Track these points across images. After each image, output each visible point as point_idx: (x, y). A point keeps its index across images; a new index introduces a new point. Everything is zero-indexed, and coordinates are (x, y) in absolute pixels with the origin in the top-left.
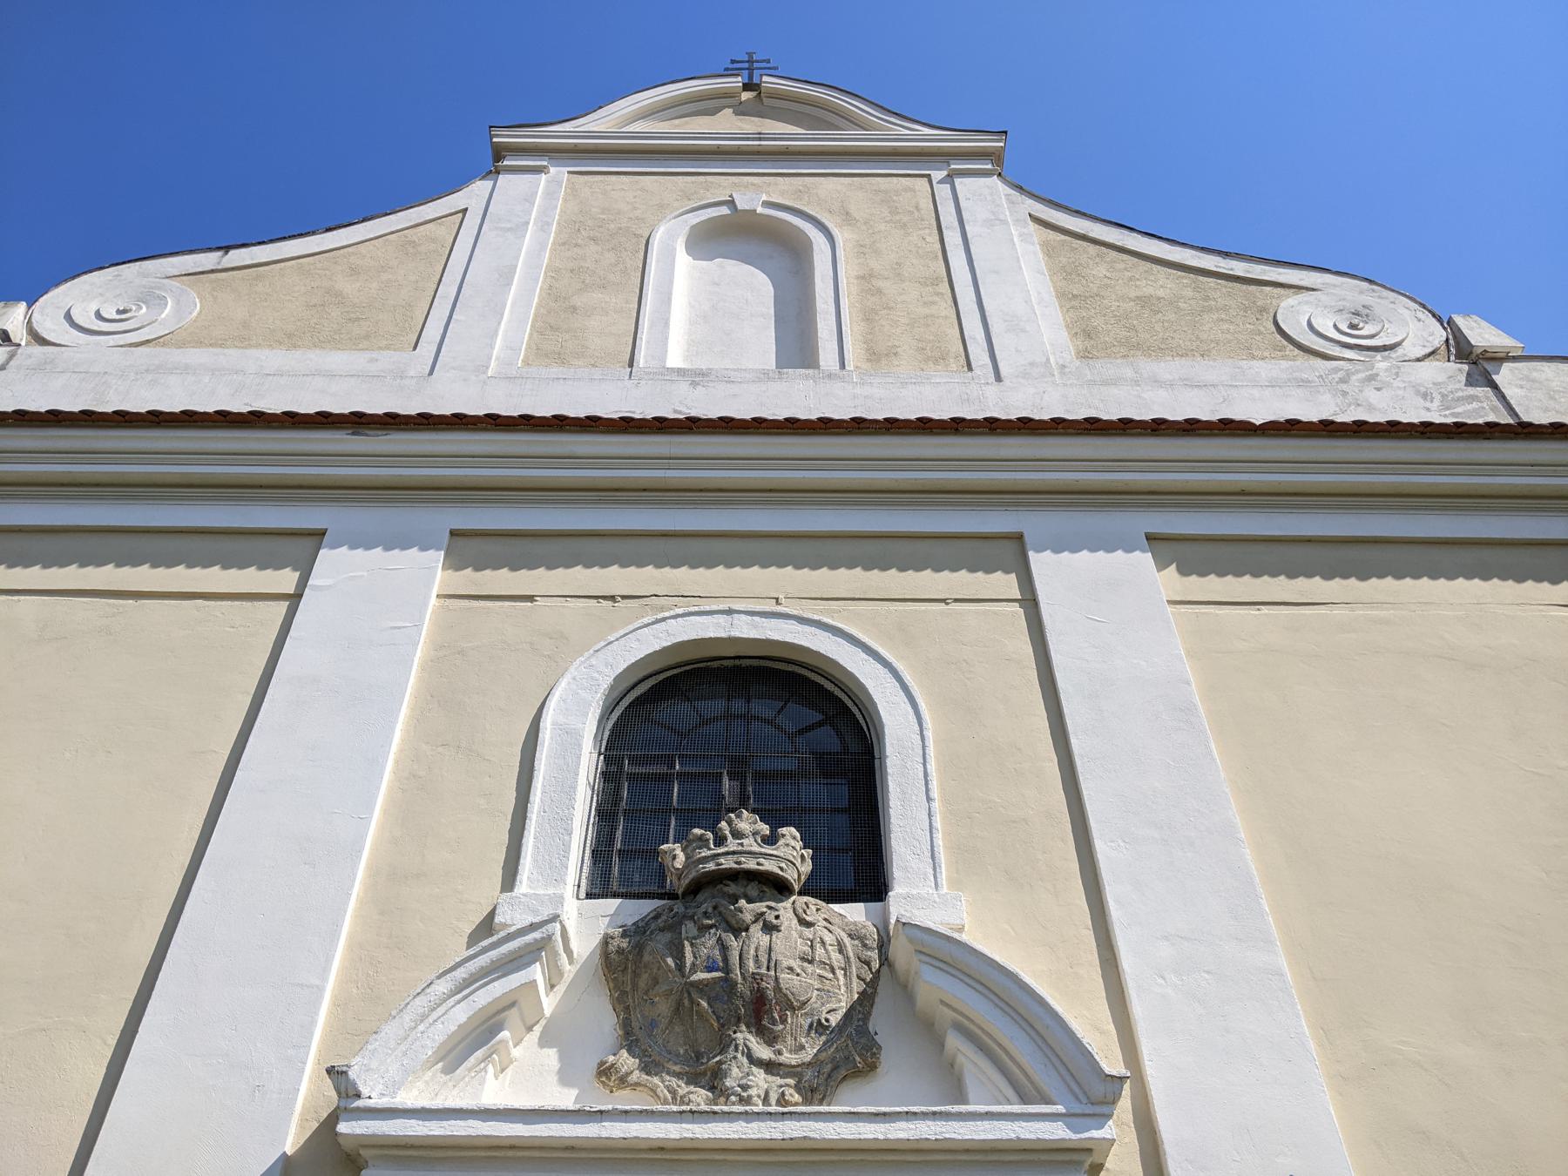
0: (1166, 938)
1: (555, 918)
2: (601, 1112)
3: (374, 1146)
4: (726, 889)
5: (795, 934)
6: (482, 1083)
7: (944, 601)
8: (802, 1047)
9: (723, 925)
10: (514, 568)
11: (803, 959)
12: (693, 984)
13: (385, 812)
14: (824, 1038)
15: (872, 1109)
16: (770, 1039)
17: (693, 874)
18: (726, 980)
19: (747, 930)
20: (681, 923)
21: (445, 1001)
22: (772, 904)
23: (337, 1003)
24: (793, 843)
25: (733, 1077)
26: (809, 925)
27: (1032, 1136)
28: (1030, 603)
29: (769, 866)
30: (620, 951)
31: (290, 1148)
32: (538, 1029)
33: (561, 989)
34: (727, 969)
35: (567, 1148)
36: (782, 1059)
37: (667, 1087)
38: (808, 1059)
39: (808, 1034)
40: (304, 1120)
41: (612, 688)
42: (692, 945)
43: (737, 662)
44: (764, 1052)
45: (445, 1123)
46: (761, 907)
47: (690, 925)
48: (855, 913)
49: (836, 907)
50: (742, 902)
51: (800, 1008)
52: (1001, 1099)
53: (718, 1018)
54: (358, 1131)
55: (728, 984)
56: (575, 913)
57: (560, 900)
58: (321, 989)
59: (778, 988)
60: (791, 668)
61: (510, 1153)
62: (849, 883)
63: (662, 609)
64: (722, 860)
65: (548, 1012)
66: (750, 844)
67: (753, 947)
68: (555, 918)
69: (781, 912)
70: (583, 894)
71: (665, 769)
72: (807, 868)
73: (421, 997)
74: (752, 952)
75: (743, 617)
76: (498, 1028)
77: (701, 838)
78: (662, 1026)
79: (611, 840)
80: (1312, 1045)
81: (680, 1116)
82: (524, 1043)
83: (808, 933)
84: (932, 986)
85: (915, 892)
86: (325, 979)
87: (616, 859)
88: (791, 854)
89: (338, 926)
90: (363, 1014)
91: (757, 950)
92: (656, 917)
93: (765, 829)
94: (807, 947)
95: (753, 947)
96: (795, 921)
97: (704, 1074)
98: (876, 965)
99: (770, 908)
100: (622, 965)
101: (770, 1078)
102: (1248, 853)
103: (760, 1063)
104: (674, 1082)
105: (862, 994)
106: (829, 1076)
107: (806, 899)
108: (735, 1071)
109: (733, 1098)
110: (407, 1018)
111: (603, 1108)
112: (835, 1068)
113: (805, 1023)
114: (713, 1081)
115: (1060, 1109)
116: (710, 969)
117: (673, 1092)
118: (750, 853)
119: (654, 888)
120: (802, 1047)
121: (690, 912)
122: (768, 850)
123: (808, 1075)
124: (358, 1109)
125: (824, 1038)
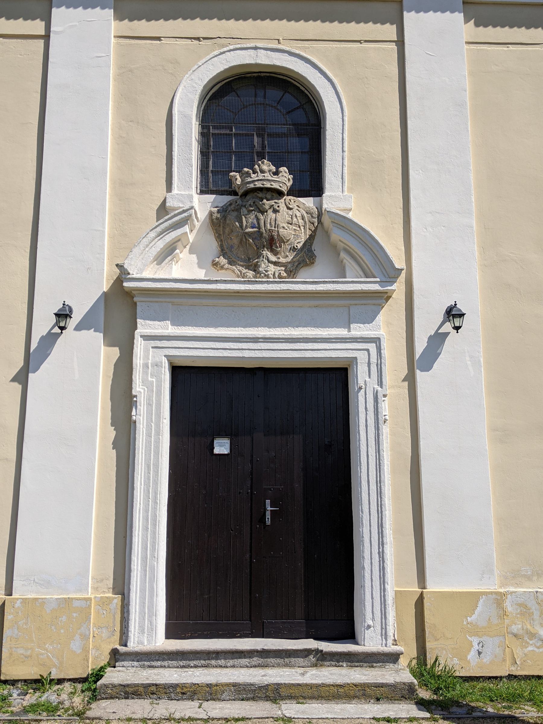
0: (431, 213)
1: (192, 208)
2: (216, 280)
3: (137, 290)
4: (258, 195)
5: (285, 213)
6: (171, 268)
7: (359, 41)
8: (287, 256)
9: (257, 210)
10: (149, 20)
11: (288, 223)
12: (246, 233)
13: (112, 154)
14: (295, 253)
15: (312, 280)
16: (276, 253)
17: (244, 189)
18: (259, 232)
19: (267, 212)
20: (241, 209)
21: (154, 239)
22: (276, 201)
23: (110, 237)
24: (285, 175)
25: (263, 266)
26: (290, 209)
27: (367, 289)
28: (400, 43)
29: (275, 186)
30: (217, 219)
31: (105, 290)
32: (188, 247)
33: (195, 232)
34: (259, 228)
35: (205, 292)
36: (280, 260)
37: (238, 270)
38: (289, 260)
39: (290, 252)
40: (108, 280)
41: (203, 91)
42: (245, 217)
43: (259, 74)
44: (273, 258)
45: (161, 283)
46: (272, 202)
47: (244, 209)
48: (309, 202)
49: (301, 199)
50: (265, 201)
51: (287, 242)
52: (359, 276)
53: (256, 246)
54: (131, 286)
55: (260, 233)
56: (197, 201)
57: (191, 197)
58: (104, 232)
59: (278, 235)
60: (285, 78)
61: (185, 293)
62: (307, 187)
63: (223, 46)
64: (256, 183)
65: (191, 241)
66: (268, 176)
67: (269, 219)
68: (192, 208)
69: (280, 205)
70: (199, 191)
71: (228, 132)
72: (289, 184)
73: (145, 238)
74: (269, 221)
75: (262, 51)
76: (174, 249)
77: (247, 173)
78: (235, 248)
79: (208, 167)
80: (477, 254)
81: (244, 282)
82: (183, 252)
83: (290, 212)
84: (336, 235)
85: (333, 194)
86: (104, 228)
87: (210, 175)
88: (284, 179)
89: (104, 206)
90: (124, 241)
91: (270, 220)
92: (231, 205)
93: (274, 169)
94: (290, 218)
95: (269, 219)
96: (285, 208)
97: (252, 265)
98: (316, 224)
99: (276, 203)
100: (219, 223)
101: (275, 267)
102: (472, 176)
103: (272, 262)
104: (241, 268)
105: (310, 235)
106: (297, 266)
107: (290, 197)
108: (263, 265)
109: (262, 275)
110: (141, 246)
111: (217, 279)
112: (299, 264)
113: (289, 248)
114: (255, 268)
115: (378, 280)
116: (253, 228)
117: (241, 272)
118: (268, 180)
119: (227, 188)
120: (287, 256)
121: (244, 204)
122: (275, 178)
123: (289, 266)
124: (129, 278)
125: (295, 253)
